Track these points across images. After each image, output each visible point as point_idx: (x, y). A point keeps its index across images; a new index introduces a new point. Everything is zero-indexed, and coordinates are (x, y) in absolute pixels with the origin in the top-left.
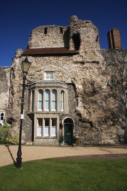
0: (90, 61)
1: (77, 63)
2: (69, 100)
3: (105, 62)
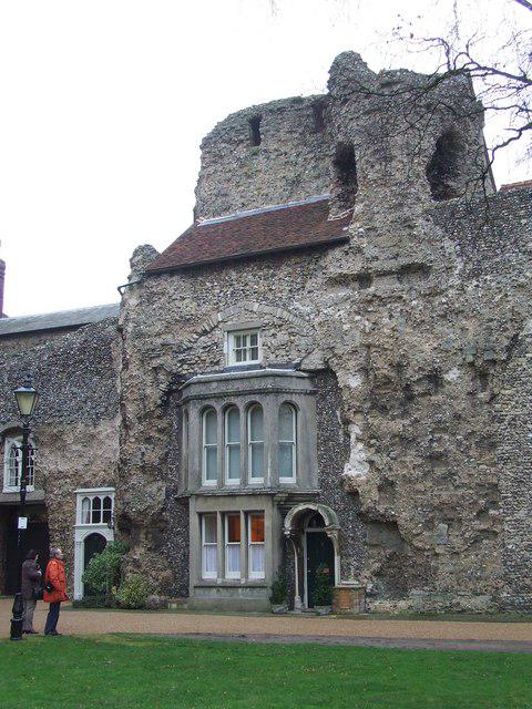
1: (341, 281)
2: (318, 438)
3: (459, 260)
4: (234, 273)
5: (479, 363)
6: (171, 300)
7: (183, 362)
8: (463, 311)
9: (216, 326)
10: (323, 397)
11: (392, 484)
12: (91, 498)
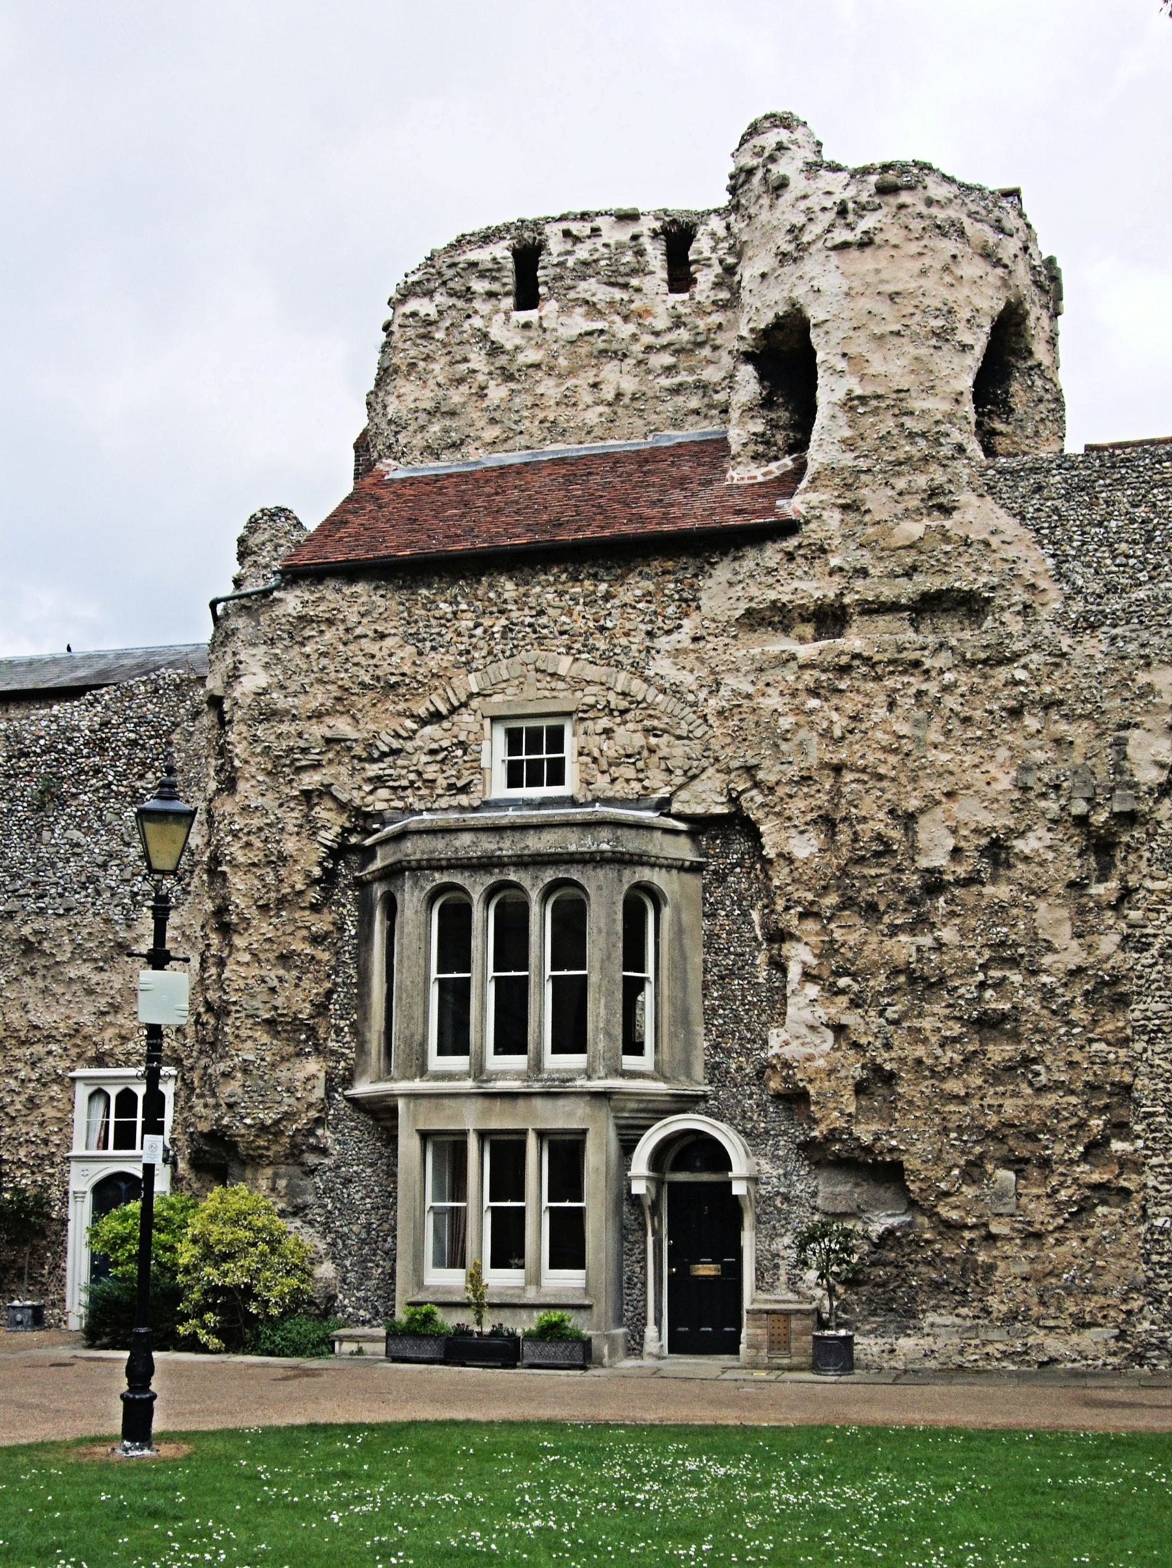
0: (906, 590)
2: (706, 971)
4: (510, 586)
5: (1100, 818)
6: (351, 637)
7: (379, 781)
8: (1061, 703)
9: (464, 705)
10: (720, 877)
11: (889, 1078)
12: (113, 1091)
